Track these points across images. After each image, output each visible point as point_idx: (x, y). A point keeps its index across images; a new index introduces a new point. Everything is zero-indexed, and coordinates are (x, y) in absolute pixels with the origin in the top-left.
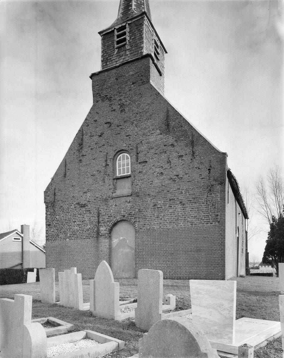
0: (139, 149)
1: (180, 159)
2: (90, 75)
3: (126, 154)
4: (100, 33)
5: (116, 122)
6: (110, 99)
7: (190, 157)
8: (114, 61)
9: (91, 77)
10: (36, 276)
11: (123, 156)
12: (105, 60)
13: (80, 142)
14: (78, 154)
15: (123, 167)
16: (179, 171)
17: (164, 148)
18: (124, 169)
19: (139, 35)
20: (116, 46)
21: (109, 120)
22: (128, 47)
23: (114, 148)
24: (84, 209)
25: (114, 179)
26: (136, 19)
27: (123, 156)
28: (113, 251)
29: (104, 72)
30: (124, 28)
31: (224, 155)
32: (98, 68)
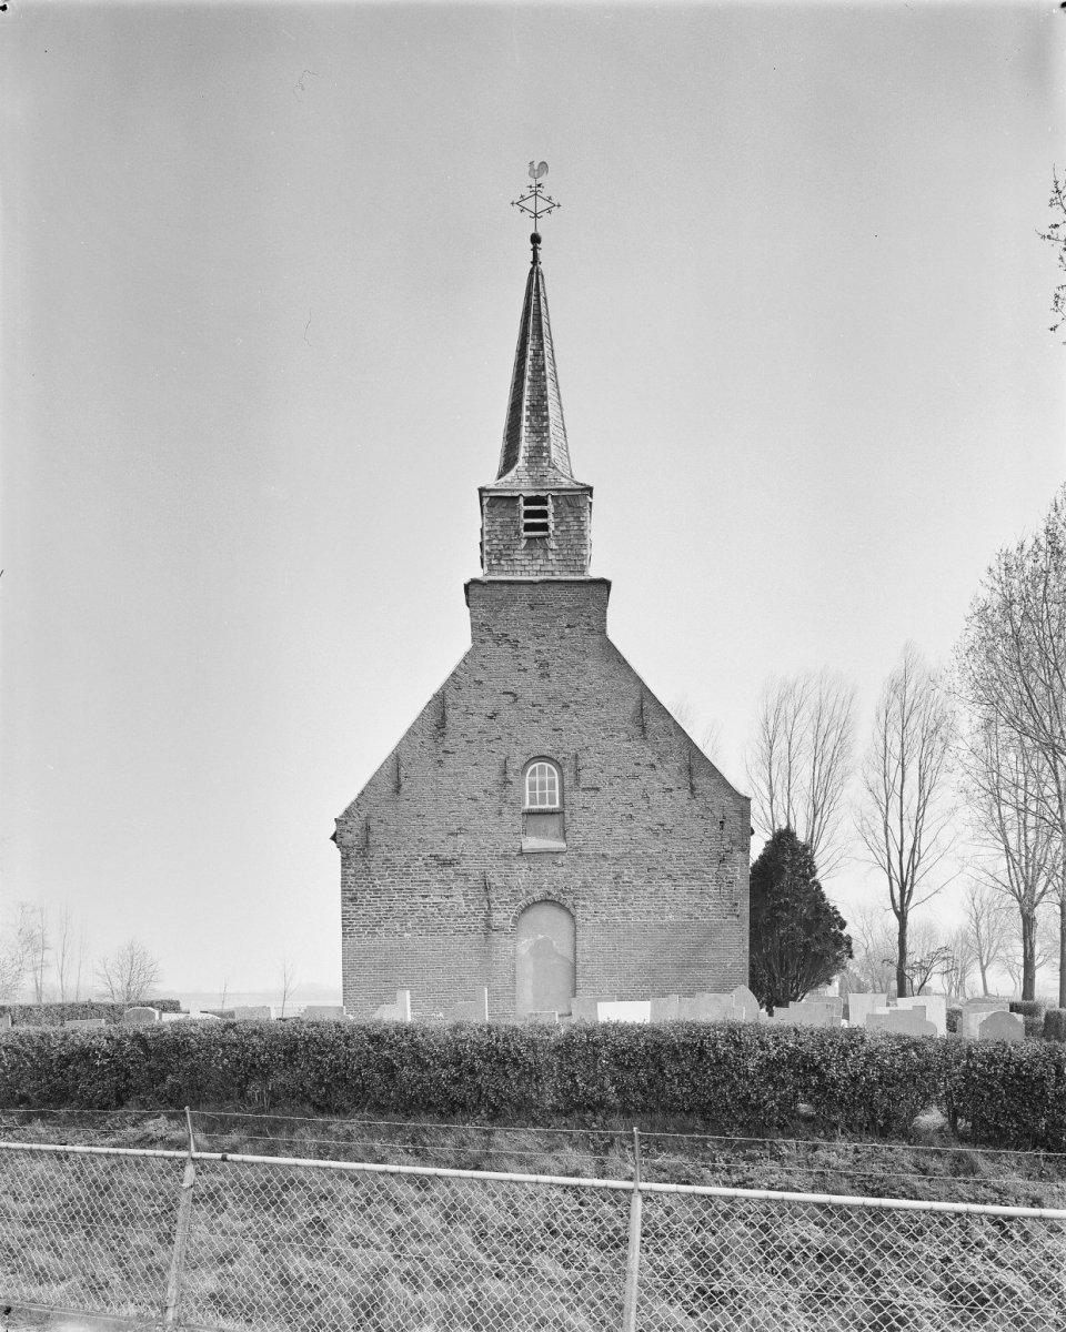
0: (581, 763)
1: (668, 794)
2: (467, 580)
3: (547, 765)
5: (529, 695)
6: (515, 644)
7: (686, 793)
8: (518, 562)
11: (542, 768)
14: (432, 747)
15: (540, 789)
16: (665, 815)
17: (636, 768)
18: (543, 796)
19: (576, 528)
21: (512, 689)
23: (526, 749)
24: (450, 870)
26: (571, 493)
27: (542, 768)
28: (729, 1017)
29: (1031, 930)
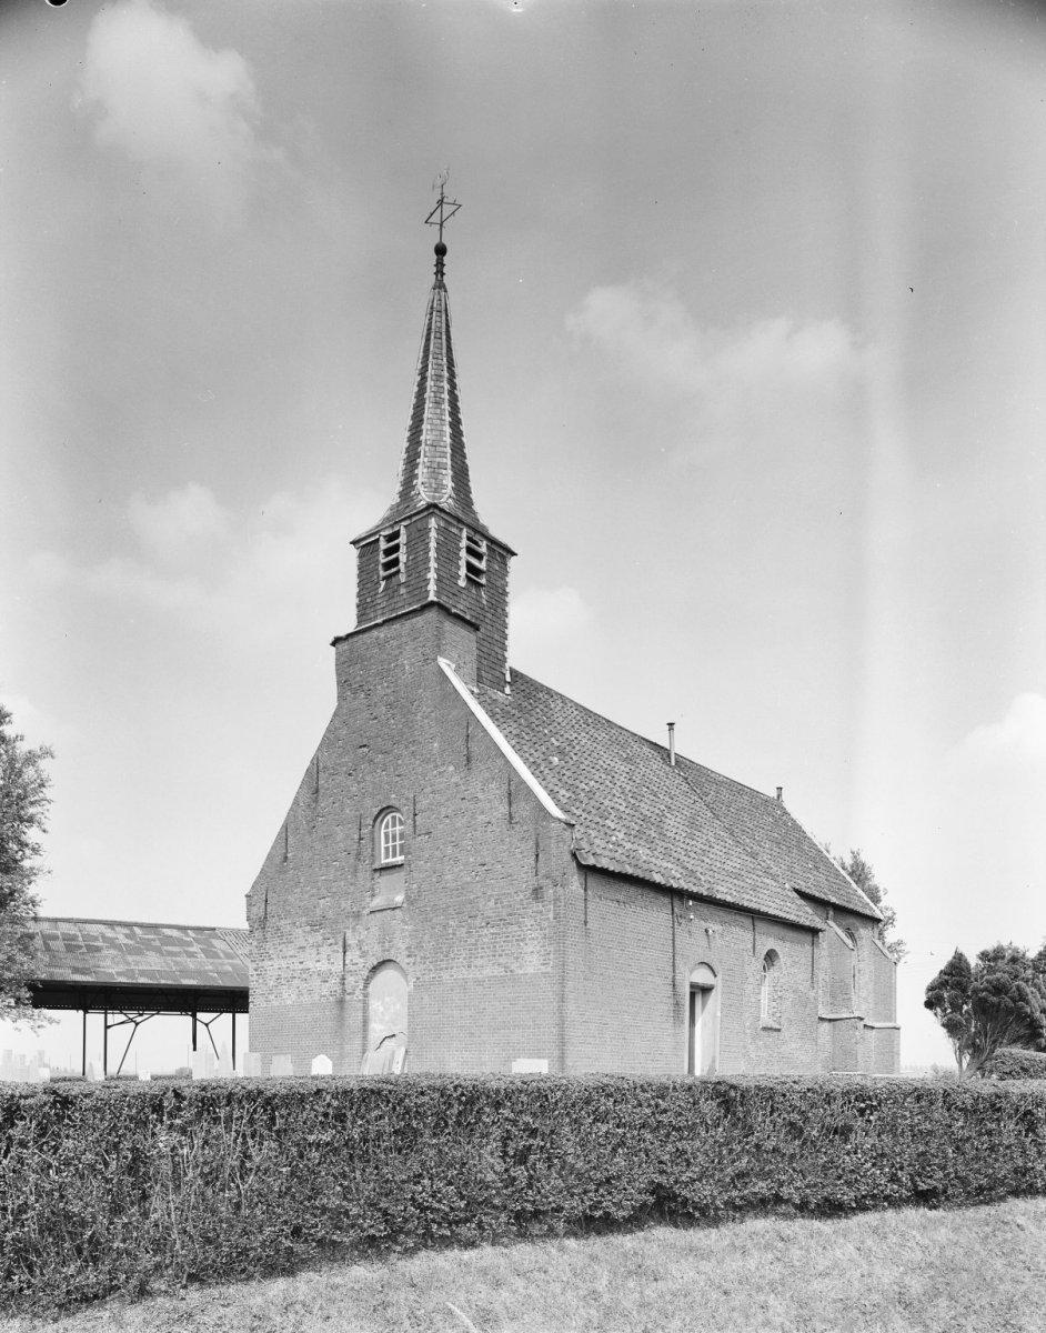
2: (331, 639)
4: (354, 543)
9: (333, 644)
10: (414, 401)
11: (394, 818)
12: (363, 609)
13: (314, 784)
20: (383, 573)
22: (402, 578)
25: (375, 870)
26: (417, 517)
30: (396, 535)
31: (929, 1004)
32: (349, 624)
